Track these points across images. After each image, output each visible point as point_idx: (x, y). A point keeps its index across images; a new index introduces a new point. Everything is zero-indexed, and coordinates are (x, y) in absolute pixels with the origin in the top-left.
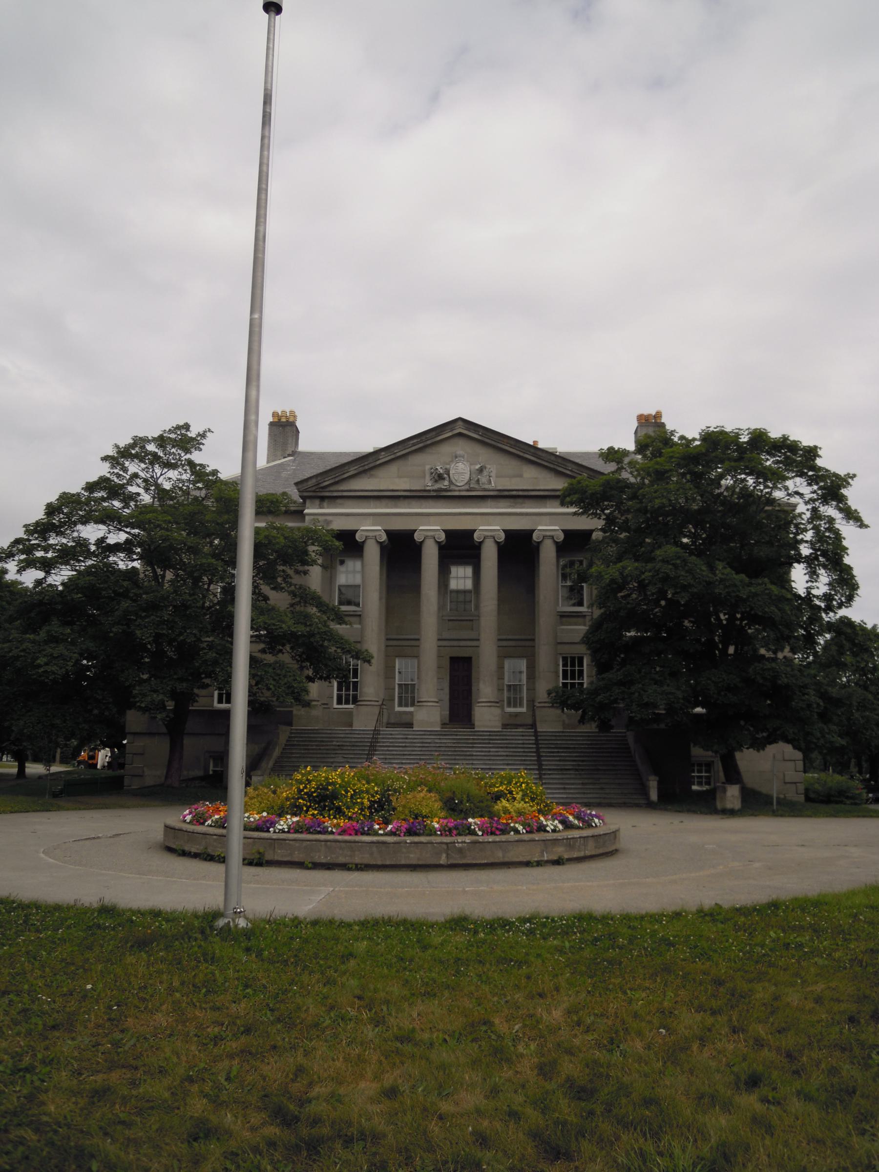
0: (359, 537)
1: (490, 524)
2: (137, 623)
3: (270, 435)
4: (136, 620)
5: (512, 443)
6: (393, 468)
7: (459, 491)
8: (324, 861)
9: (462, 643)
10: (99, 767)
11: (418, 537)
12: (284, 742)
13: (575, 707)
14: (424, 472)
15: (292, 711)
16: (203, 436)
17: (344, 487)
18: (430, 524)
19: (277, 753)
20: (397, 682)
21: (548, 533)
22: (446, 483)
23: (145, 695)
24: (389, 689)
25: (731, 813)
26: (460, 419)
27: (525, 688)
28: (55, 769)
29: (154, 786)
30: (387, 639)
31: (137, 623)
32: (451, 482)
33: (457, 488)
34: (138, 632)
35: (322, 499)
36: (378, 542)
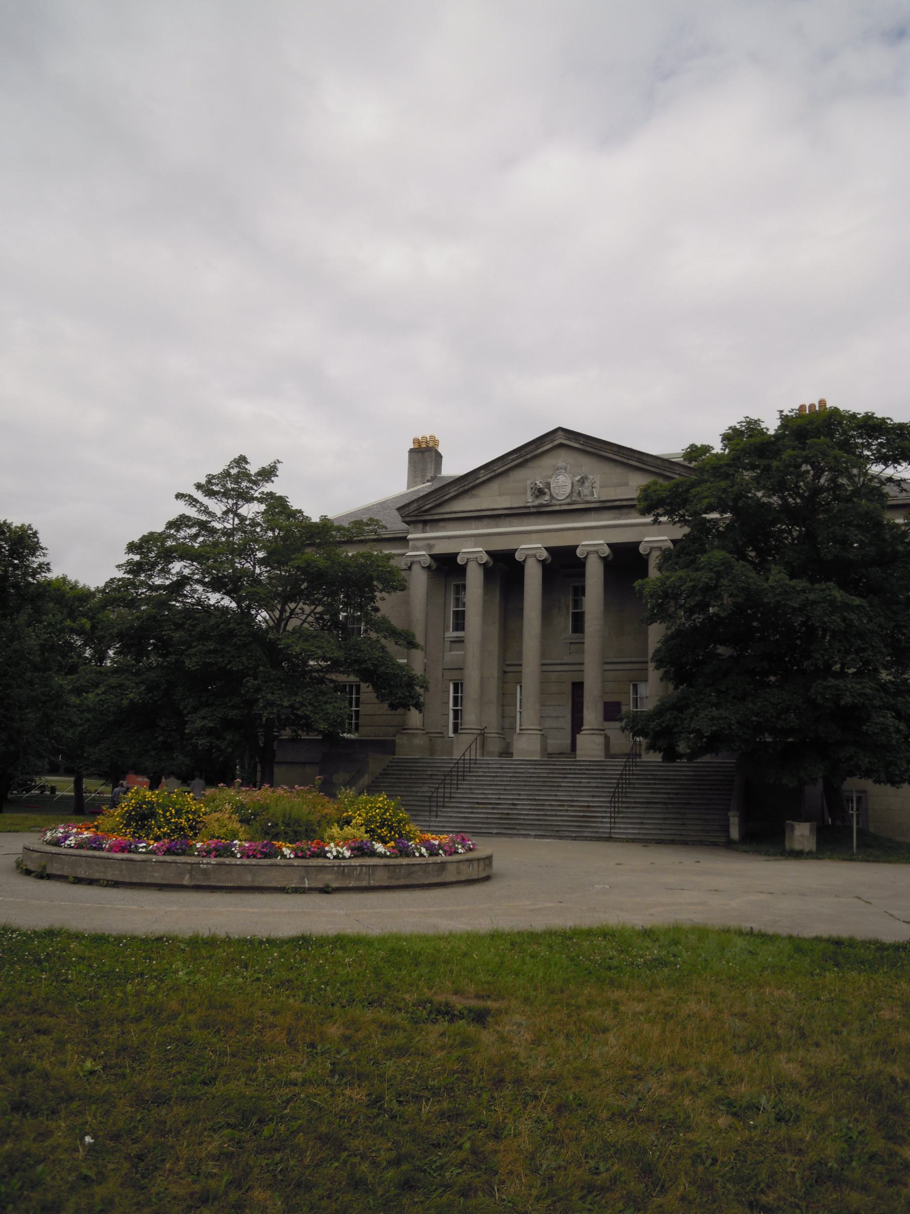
0: (460, 560)
1: (532, 542)
3: (410, 462)
5: (615, 449)
6: (495, 486)
7: (560, 505)
8: (83, 876)
11: (518, 557)
15: (394, 741)
21: (656, 545)
22: (547, 498)
25: (798, 855)
26: (560, 429)
30: (543, 665)
32: (552, 497)
34: (187, 662)
35: (425, 522)
36: (601, 557)
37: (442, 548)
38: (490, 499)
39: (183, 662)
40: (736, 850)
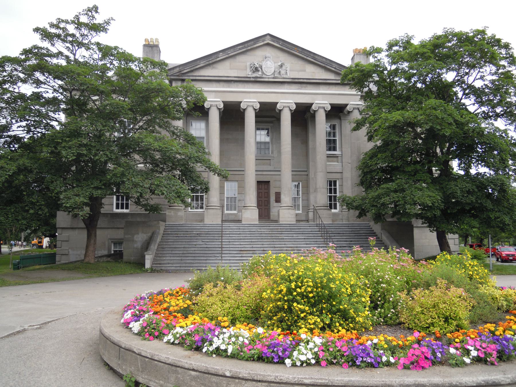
1: (287, 99)
2: (63, 145)
4: (62, 143)
5: (300, 50)
6: (227, 63)
9: (265, 173)
10: (44, 247)
11: (243, 106)
12: (162, 232)
13: (356, 208)
14: (246, 66)
16: (108, 23)
17: (197, 73)
18: (250, 98)
19: (159, 240)
20: (225, 196)
21: (321, 105)
22: (260, 73)
23: (69, 198)
24: (222, 200)
27: (301, 199)
28: (15, 249)
29: (76, 262)
31: (63, 145)
32: (262, 72)
33: (268, 77)
34: (64, 153)
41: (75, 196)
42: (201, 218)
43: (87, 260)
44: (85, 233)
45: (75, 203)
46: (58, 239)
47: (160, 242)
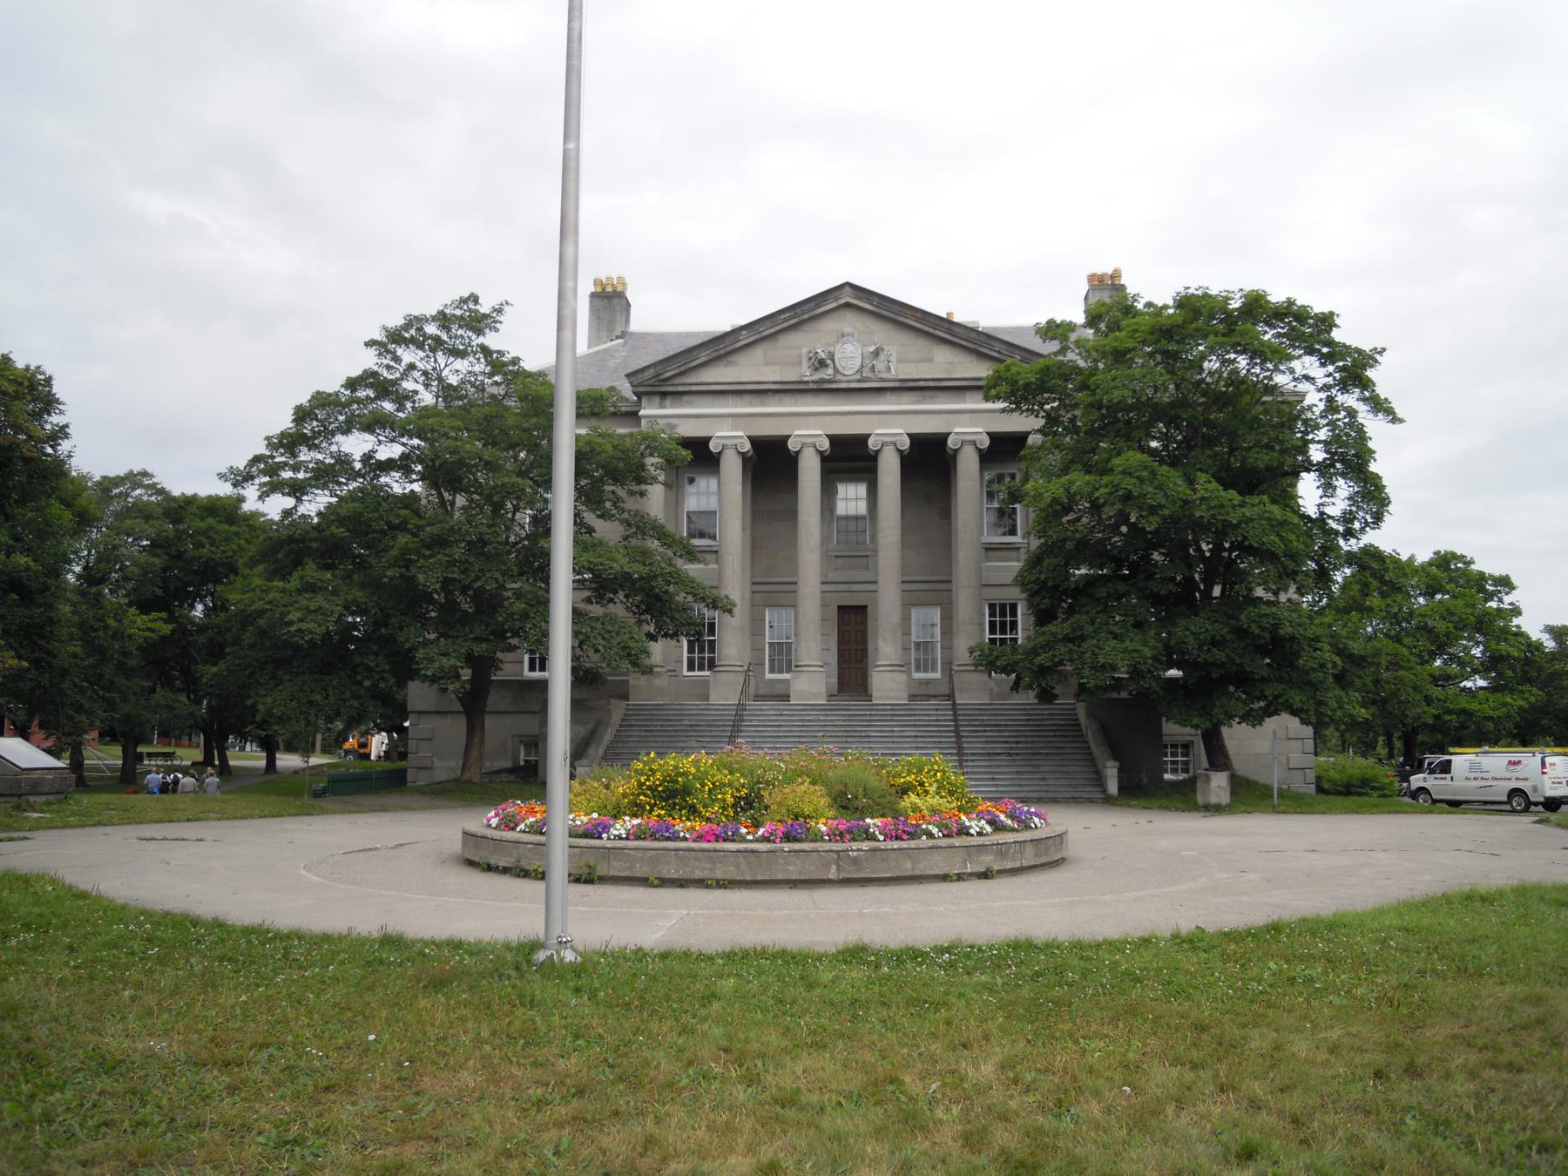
1: (889, 427)
6: (758, 353)
9: (855, 587)
11: (792, 445)
13: (1006, 670)
14: (800, 357)
18: (809, 427)
22: (830, 371)
25: (1217, 809)
32: (836, 370)
34: (421, 578)
35: (664, 395)
37: (688, 430)
38: (750, 368)
39: (414, 577)
40: (1114, 804)
41: (437, 653)
42: (703, 691)
43: (466, 776)
44: (462, 723)
45: (442, 669)
46: (411, 734)
47: (612, 742)
